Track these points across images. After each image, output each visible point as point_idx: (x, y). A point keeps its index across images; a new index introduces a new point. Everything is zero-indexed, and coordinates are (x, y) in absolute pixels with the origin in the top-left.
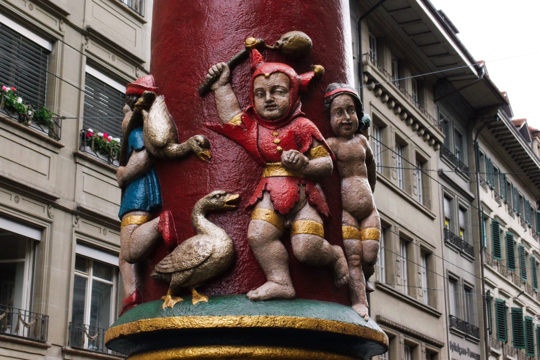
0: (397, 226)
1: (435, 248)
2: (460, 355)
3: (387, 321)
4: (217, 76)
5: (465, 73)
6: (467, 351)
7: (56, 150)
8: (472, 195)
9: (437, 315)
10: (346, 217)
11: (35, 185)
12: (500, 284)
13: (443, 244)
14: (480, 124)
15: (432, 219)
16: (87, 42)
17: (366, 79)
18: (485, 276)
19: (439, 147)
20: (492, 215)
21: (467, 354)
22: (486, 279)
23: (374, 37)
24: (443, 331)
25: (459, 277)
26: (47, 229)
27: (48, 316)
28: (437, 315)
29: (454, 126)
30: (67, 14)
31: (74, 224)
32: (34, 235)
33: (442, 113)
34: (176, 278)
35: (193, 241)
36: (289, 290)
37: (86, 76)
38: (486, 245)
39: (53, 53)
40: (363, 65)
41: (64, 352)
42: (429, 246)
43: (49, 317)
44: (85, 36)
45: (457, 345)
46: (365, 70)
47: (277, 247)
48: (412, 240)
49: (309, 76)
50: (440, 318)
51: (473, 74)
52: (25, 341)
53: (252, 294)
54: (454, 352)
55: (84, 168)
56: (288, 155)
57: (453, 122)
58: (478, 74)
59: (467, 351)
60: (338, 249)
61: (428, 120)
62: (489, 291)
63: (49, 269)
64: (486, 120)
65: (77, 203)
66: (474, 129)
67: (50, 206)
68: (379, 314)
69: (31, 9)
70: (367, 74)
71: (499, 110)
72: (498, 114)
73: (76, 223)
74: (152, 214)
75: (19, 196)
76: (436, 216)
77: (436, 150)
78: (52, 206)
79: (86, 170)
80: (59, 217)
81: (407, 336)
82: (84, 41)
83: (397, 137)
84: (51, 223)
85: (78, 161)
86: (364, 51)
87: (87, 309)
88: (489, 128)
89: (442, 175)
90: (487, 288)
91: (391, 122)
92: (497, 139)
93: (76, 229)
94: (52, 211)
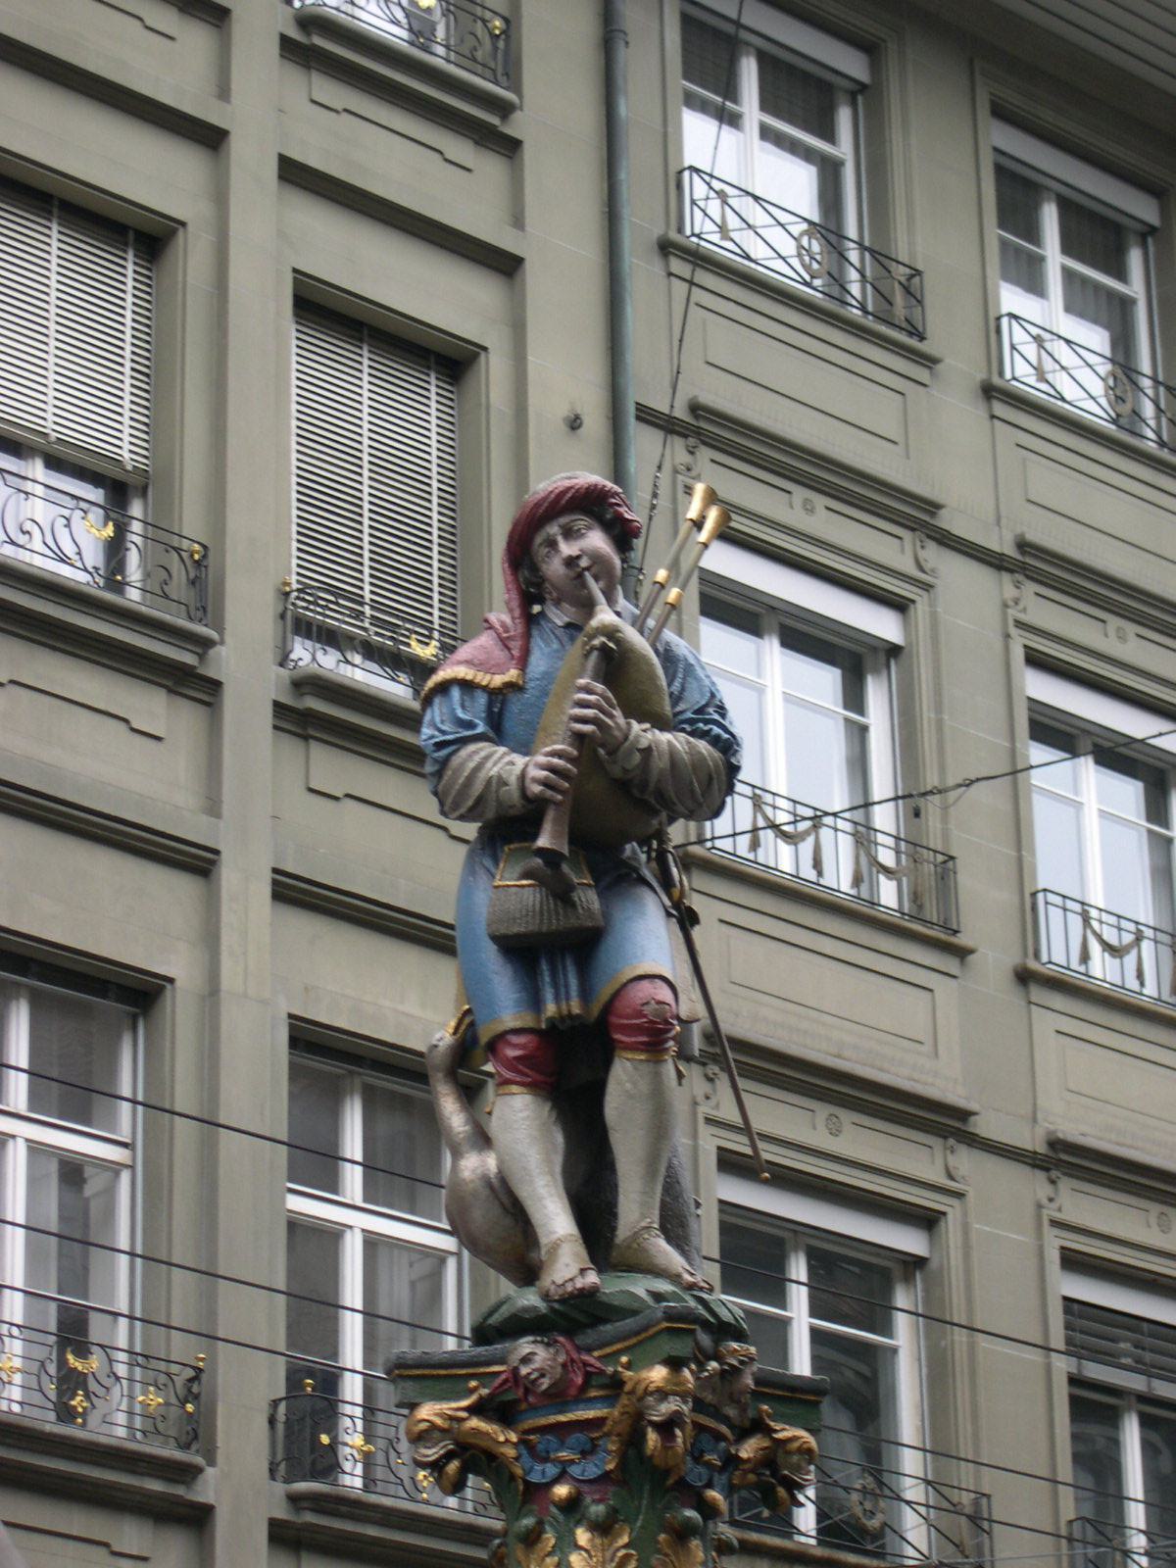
16: (1056, 1191)
26: (950, 1217)
27: (988, 1496)
30: (964, 1115)
32: (906, 1240)
37: (1067, 1311)
39: (934, 1264)
43: (926, 277)
44: (1047, 1170)
55: (1021, 434)
69: (835, 1133)
73: (1051, 1200)
80: (954, 573)
82: (1010, 592)
85: (997, 413)
87: (1129, 1459)
93: (1049, 1212)
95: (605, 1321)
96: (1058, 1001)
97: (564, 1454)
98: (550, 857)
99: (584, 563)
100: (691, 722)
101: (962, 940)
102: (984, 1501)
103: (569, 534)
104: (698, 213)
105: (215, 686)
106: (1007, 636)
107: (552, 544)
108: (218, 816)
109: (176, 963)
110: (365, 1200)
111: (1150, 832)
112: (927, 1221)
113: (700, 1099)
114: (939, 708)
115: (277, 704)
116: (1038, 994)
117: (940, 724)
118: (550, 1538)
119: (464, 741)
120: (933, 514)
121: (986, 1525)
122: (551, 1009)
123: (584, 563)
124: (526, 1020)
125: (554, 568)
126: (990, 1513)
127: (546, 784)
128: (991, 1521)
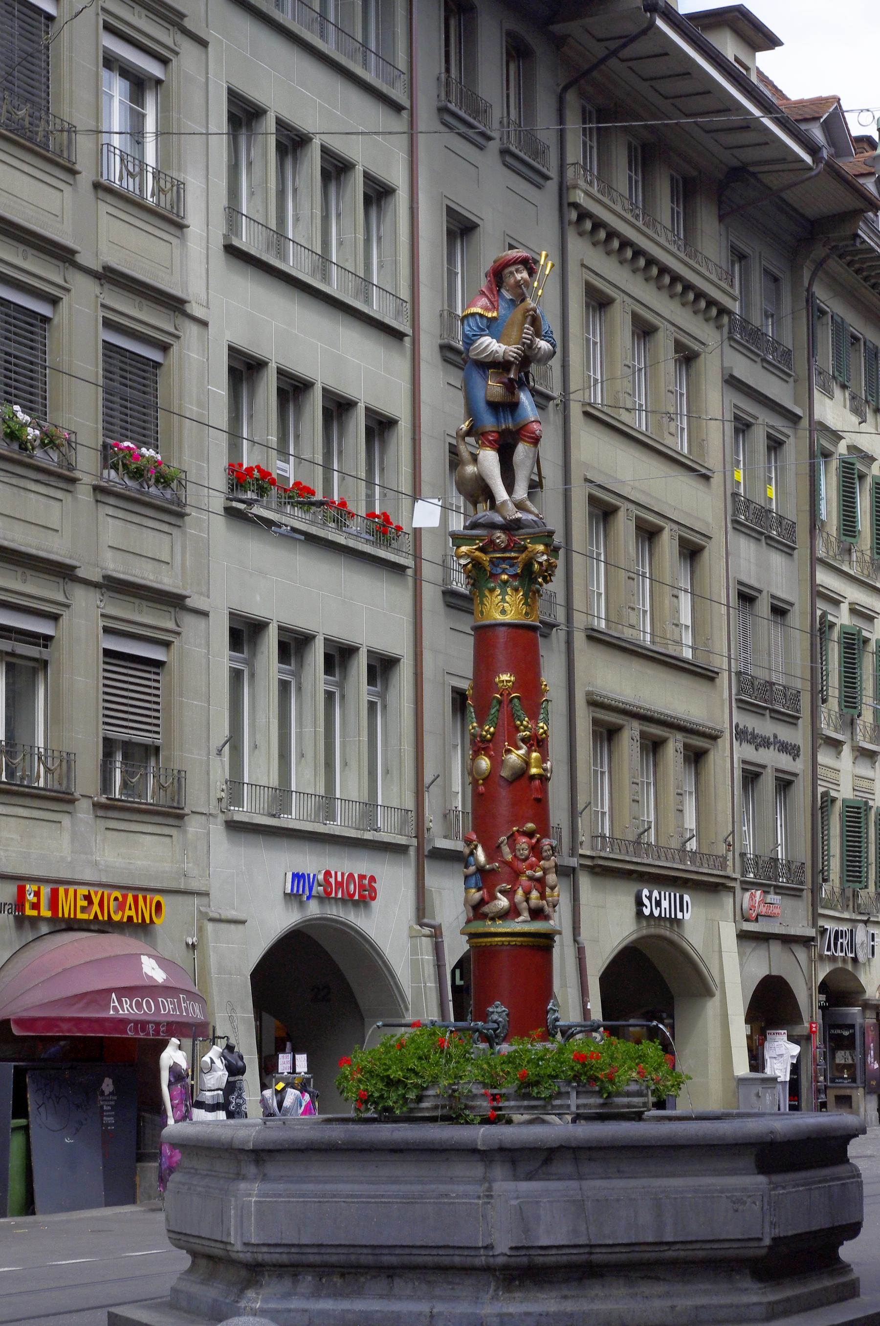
1: (710, 538)
2: (757, 750)
4: (502, 842)
5: (785, 159)
6: (772, 739)
7: (70, 488)
8: (798, 411)
9: (707, 676)
10: (548, 889)
11: (46, 551)
12: (853, 594)
13: (729, 525)
14: (820, 251)
15: (706, 478)
17: (574, 215)
18: (818, 582)
20: (842, 448)
21: (772, 747)
22: (821, 589)
23: (592, 109)
24: (723, 705)
25: (760, 591)
26: (64, 300)
28: (707, 676)
30: (73, 252)
31: (99, 603)
33: (734, 241)
35: (496, 902)
36: (529, 919)
38: (823, 517)
40: (568, 189)
42: (698, 536)
44: (100, 279)
45: (750, 730)
46: (571, 200)
47: (525, 904)
49: (534, 841)
50: (717, 680)
51: (803, 161)
52: (48, 793)
53: (516, 920)
54: (744, 745)
55: (107, 507)
56: (529, 872)
57: (760, 253)
58: (813, 162)
59: (772, 739)
60: (544, 902)
61: (703, 270)
62: (824, 615)
64: (833, 244)
66: (808, 262)
67: (67, 580)
70: (575, 205)
71: (861, 224)
72: (860, 232)
74: (479, 889)
77: (719, 327)
78: (70, 580)
79: (111, 511)
81: (645, 723)
86: (570, 159)
88: (841, 256)
89: (732, 382)
90: (822, 606)
91: (624, 292)
92: (859, 277)
94: (70, 586)
95: (522, 528)
96: (109, 198)
97: (504, 566)
98: (510, 380)
99: (522, 282)
100: (545, 336)
103: (517, 271)
104: (725, 267)
106: (98, 14)
107: (512, 273)
111: (131, 108)
116: (101, 194)
118: (498, 591)
119: (482, 336)
120: (182, 19)
121: (73, 445)
122: (504, 427)
123: (522, 282)
127: (515, 358)
128: (76, 443)
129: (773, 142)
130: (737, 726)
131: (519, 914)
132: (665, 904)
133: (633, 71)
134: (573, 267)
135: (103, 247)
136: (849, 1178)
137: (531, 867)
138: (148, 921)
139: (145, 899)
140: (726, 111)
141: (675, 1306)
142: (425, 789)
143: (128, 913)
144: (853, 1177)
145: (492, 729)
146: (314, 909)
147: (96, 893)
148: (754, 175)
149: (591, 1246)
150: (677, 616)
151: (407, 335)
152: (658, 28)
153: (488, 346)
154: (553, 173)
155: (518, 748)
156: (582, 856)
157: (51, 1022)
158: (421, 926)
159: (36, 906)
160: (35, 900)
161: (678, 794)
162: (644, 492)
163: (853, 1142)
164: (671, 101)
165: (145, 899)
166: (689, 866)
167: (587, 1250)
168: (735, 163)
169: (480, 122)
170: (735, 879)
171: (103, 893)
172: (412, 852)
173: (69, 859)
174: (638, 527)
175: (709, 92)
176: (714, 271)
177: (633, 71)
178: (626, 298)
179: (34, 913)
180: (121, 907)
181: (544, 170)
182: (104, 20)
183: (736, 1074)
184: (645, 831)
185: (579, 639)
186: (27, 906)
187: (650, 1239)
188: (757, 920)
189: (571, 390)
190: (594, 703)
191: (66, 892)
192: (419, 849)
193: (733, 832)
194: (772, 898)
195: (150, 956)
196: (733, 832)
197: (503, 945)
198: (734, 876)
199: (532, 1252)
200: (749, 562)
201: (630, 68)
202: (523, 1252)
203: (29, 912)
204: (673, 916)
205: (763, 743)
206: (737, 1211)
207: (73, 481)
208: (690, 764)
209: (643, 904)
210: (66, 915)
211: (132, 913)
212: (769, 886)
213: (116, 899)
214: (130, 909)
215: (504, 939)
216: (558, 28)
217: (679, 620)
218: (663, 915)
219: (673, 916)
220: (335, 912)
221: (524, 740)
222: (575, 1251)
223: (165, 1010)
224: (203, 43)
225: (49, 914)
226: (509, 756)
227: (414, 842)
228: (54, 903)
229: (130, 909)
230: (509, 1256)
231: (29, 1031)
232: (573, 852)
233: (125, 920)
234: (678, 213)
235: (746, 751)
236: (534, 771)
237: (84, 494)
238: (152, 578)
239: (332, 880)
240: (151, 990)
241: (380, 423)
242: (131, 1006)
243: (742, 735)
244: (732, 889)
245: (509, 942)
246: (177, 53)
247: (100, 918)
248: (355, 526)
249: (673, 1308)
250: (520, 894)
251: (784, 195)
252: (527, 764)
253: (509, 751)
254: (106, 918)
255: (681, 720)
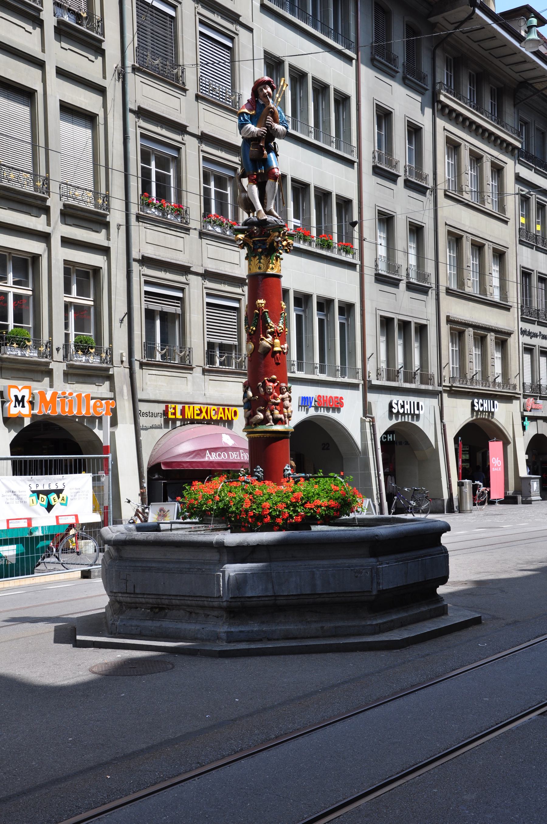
0: (468, 235)
1: (508, 248)
2: (531, 338)
3: (456, 319)
5: (544, 76)
6: (538, 334)
9: (507, 308)
11: (176, 260)
19: (516, 152)
25: (533, 271)
29: (536, 125)
34: (254, 422)
35: (256, 416)
39: (179, 158)
41: (204, 371)
45: (528, 330)
48: (484, 245)
49: (276, 384)
54: (525, 336)
59: (538, 334)
63: (190, 315)
65: (204, 267)
68: (448, 315)
70: (441, 102)
75: (166, 269)
76: (509, 219)
83: (472, 152)
84: (188, 284)
89: (519, 179)
101: (186, 87)
102: (188, 209)
104: (516, 128)
105: (42, 21)
106: (195, 16)
108: (44, 53)
109: (38, 86)
110: (77, 295)
112: (182, 290)
113: (137, 121)
114: (182, 33)
115: (55, 26)
117: (182, 36)
124: (105, 193)
125: (261, 94)
126: (186, 189)
129: (538, 67)
130: (521, 329)
131: (268, 422)
132: (485, 405)
133: (469, 38)
134: (439, 130)
135: (202, 124)
136: (438, 554)
137: (275, 398)
138: (230, 419)
139: (228, 409)
140: (525, 62)
141: (324, 627)
142: (367, 360)
143: (220, 416)
144: (442, 553)
145: (254, 328)
146: (312, 412)
147: (204, 407)
148: (531, 84)
149: (276, 596)
150: (491, 282)
151: (356, 162)
152: (478, 15)
153: (249, 129)
154: (429, 87)
155: (267, 337)
156: (444, 386)
157: (179, 463)
158: (366, 418)
159: (174, 414)
160: (173, 411)
161: (492, 358)
162: (475, 229)
163: (443, 535)
164: (488, 51)
165: (228, 409)
166: (497, 389)
167: (273, 598)
168: (521, 79)
169: (392, 65)
170: (520, 394)
171: (207, 407)
172: (361, 387)
173: (191, 393)
174: (472, 244)
175: (505, 45)
176: (510, 129)
177: (469, 38)
178: (466, 144)
179: (173, 417)
180: (217, 413)
181: (425, 86)
182: (199, 18)
183: (520, 476)
184: (475, 375)
185: (443, 295)
186: (170, 413)
187: (308, 592)
188: (530, 411)
189: (438, 184)
190: (449, 320)
191: (189, 407)
192: (364, 385)
193: (519, 373)
194: (539, 401)
195: (226, 434)
196: (519, 373)
197: (260, 437)
198: (519, 392)
199: (242, 600)
200: (528, 258)
201: (468, 36)
202: (238, 600)
203: (170, 416)
204: (489, 410)
205: (534, 335)
206: (357, 577)
207: (188, 230)
208: (499, 346)
209: (475, 406)
210: (189, 417)
211: (222, 416)
212: (537, 396)
213: (214, 410)
214: (221, 414)
215: (260, 434)
216: (432, 19)
217: (492, 284)
218: (484, 410)
219: (489, 410)
220: (322, 412)
221: (270, 333)
222: (267, 599)
223: (232, 457)
224: (250, 30)
225: (181, 417)
226: (263, 341)
227: (362, 382)
228: (183, 412)
229: (221, 414)
230: (230, 602)
231: (169, 468)
232: (440, 385)
233: (219, 418)
234: (494, 105)
235: (527, 339)
236: (277, 349)
237: (194, 234)
238: (230, 271)
239: (322, 400)
240: (226, 449)
241: (345, 201)
242: (216, 456)
243: (524, 332)
244: (518, 399)
245: (263, 436)
246: (237, 34)
247: (206, 418)
248: (314, 244)
249: (322, 628)
250: (268, 413)
251: (544, 92)
252: (273, 346)
253: (262, 339)
254: (209, 418)
255: (493, 327)
